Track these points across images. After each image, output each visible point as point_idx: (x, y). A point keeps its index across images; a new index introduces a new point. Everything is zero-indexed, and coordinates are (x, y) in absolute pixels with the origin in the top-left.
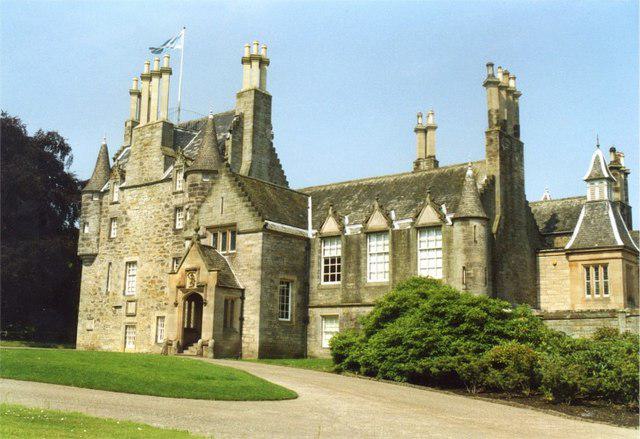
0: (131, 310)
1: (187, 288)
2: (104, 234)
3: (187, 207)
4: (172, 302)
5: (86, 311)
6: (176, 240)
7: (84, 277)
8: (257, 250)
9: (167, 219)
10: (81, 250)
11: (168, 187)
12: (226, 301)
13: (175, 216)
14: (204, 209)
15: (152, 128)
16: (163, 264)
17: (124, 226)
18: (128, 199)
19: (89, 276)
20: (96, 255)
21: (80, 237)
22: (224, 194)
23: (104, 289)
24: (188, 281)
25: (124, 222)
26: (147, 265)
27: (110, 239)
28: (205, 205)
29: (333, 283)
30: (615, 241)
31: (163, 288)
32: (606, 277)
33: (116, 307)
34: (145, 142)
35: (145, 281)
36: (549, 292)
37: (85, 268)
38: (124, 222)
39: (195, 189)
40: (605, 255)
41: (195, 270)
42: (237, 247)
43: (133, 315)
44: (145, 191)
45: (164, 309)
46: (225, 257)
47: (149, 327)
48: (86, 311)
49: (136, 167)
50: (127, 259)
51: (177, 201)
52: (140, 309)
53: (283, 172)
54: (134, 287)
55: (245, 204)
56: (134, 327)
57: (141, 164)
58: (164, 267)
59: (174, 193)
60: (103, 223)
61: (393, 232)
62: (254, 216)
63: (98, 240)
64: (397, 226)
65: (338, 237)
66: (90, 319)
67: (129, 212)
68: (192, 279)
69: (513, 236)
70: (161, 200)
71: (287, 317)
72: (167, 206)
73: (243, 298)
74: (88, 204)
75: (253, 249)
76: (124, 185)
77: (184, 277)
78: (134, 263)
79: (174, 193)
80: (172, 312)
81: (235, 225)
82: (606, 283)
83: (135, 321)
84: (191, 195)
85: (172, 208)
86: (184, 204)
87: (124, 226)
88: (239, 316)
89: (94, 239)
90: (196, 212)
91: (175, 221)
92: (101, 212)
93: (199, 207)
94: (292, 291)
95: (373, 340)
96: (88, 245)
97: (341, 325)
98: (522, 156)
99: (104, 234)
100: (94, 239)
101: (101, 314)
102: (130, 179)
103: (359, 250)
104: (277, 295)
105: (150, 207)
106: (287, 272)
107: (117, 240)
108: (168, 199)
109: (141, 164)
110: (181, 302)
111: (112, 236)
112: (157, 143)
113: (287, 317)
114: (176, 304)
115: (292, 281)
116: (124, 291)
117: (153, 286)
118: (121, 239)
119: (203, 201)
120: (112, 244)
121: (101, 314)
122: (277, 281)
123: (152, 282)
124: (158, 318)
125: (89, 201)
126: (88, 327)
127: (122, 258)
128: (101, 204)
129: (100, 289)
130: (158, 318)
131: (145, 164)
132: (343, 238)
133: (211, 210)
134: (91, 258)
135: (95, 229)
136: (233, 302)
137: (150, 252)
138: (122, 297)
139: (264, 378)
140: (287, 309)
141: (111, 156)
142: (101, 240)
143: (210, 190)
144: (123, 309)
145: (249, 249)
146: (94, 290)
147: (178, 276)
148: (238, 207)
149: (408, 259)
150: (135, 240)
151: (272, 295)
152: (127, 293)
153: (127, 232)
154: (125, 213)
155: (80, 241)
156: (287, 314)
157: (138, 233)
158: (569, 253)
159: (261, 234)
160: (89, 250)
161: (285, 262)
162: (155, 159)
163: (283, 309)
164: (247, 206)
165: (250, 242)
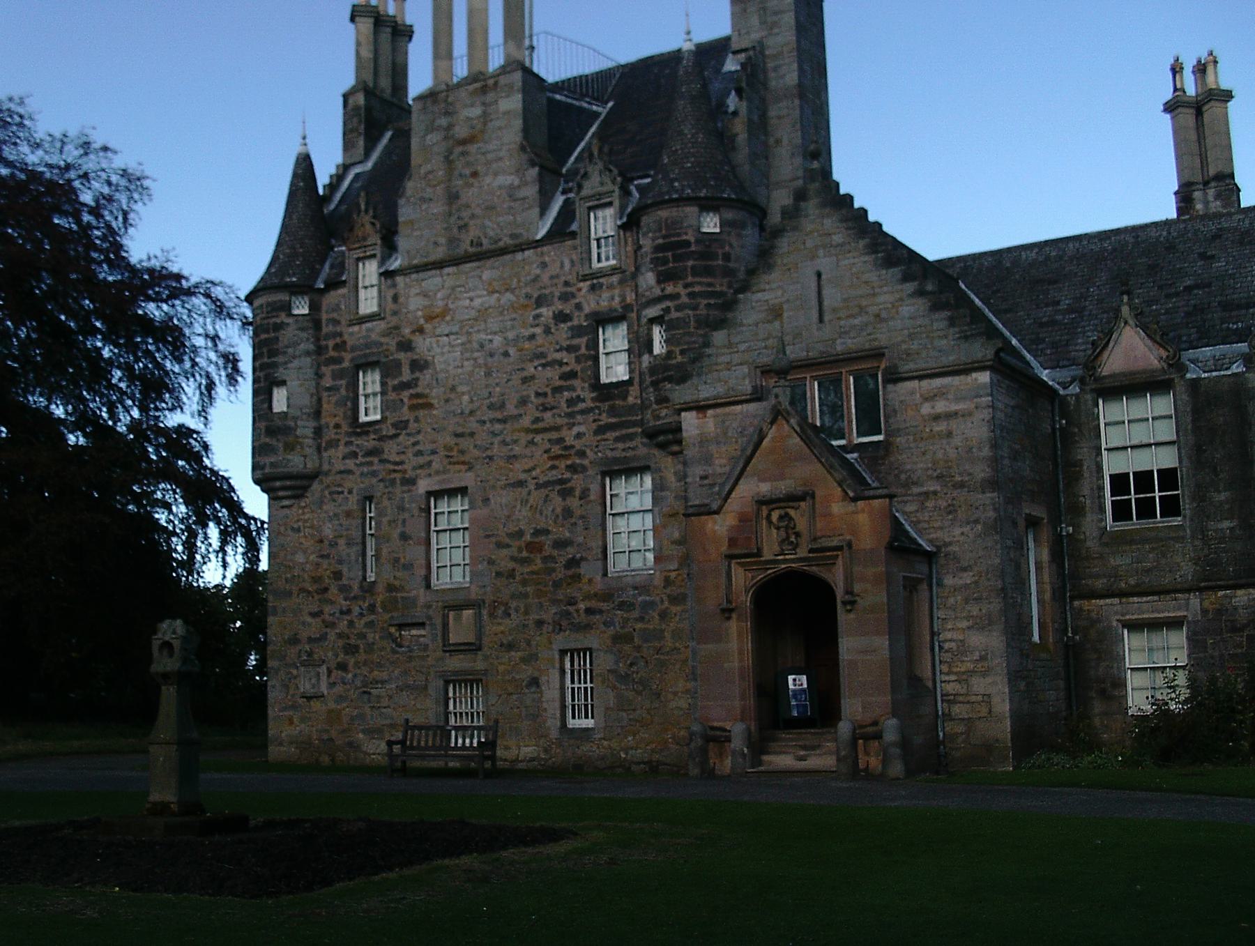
1: (767, 555)
6: (605, 419)
8: (976, 430)
9: (564, 356)
13: (594, 345)
16: (566, 493)
18: (415, 304)
25: (406, 375)
29: (1147, 523)
31: (573, 563)
34: (461, 131)
35: (500, 545)
38: (406, 375)
41: (793, 499)
45: (587, 627)
47: (535, 682)
48: (294, 640)
49: (438, 208)
53: (863, 212)
55: (910, 287)
57: (452, 197)
58: (574, 503)
60: (327, 382)
62: (952, 322)
63: (318, 432)
70: (540, 301)
72: (561, 317)
76: (395, 264)
83: (480, 665)
89: (305, 429)
92: (320, 350)
95: (385, 676)
96: (290, 447)
97: (1195, 643)
99: (332, 413)
100: (305, 429)
107: (387, 430)
108: (565, 297)
109: (452, 197)
116: (427, 579)
118: (401, 425)
120: (368, 442)
123: (530, 547)
124: (563, 653)
127: (412, 482)
129: (338, 575)
130: (563, 653)
132: (1180, 386)
142: (330, 434)
145: (941, 427)
146: (316, 580)
148: (885, 299)
153: (422, 403)
154: (406, 346)
159: (984, 377)
164: (920, 293)
165: (941, 406)
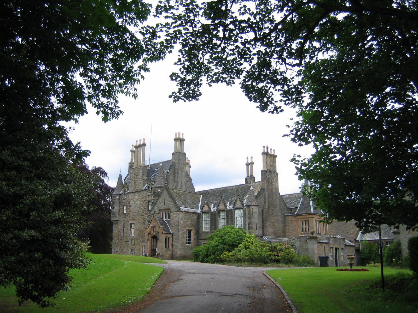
0: (133, 243)
2: (121, 212)
3: (152, 201)
4: (147, 239)
5: (115, 243)
7: (114, 229)
9: (145, 206)
10: (112, 219)
11: (145, 193)
12: (166, 238)
13: (148, 205)
14: (158, 203)
15: (139, 168)
16: (144, 224)
17: (129, 209)
19: (116, 230)
20: (118, 220)
21: (112, 213)
22: (165, 197)
23: (122, 235)
24: (152, 231)
26: (138, 224)
27: (124, 214)
28: (159, 201)
30: (311, 211)
32: (308, 225)
33: (127, 242)
35: (137, 231)
36: (290, 231)
37: (114, 226)
39: (155, 194)
40: (308, 216)
42: (170, 218)
43: (134, 245)
44: (137, 194)
46: (166, 222)
47: (140, 249)
48: (115, 243)
50: (130, 222)
51: (149, 199)
52: (136, 242)
54: (133, 233)
56: (134, 249)
57: (135, 183)
59: (148, 196)
61: (227, 210)
63: (119, 214)
64: (228, 208)
65: (208, 212)
66: (117, 247)
67: (131, 203)
68: (154, 231)
69: (273, 210)
71: (190, 244)
72: (145, 201)
73: (172, 237)
74: (115, 200)
75: (176, 218)
77: (151, 230)
78: (133, 223)
79: (148, 196)
80: (147, 243)
81: (169, 209)
82: (308, 227)
83: (135, 247)
84: (154, 197)
85: (147, 201)
86: (151, 200)
87: (129, 209)
88: (171, 244)
89: (117, 214)
90: (155, 204)
91: (148, 206)
92: (120, 203)
93: (156, 202)
94: (192, 234)
96: (115, 216)
98: (278, 178)
100: (117, 214)
101: (121, 245)
102: (131, 189)
103: (215, 218)
104: (186, 236)
105: (139, 201)
106: (189, 227)
107: (126, 214)
109: (135, 183)
110: (150, 239)
111: (125, 213)
112: (141, 175)
113: (190, 244)
114: (148, 240)
115: (192, 230)
117: (140, 233)
118: (128, 214)
119: (158, 200)
120: (124, 216)
121: (121, 245)
122: (185, 230)
123: (141, 231)
125: (115, 198)
126: (116, 250)
127: (129, 222)
128: (120, 199)
129: (120, 234)
131: (137, 183)
133: (161, 203)
134: (117, 221)
135: (117, 210)
136: (169, 239)
137: (139, 219)
138: (129, 238)
139: (277, 268)
140: (190, 241)
141: (123, 178)
142: (120, 215)
143: (160, 195)
144: (130, 243)
146: (118, 235)
147: (148, 229)
149: (232, 221)
150: (133, 214)
151: (183, 236)
152: (131, 236)
154: (129, 203)
155: (112, 215)
156: (190, 243)
157: (134, 211)
158: (296, 215)
160: (116, 219)
161: (188, 223)
162: (140, 181)
163: (188, 241)
